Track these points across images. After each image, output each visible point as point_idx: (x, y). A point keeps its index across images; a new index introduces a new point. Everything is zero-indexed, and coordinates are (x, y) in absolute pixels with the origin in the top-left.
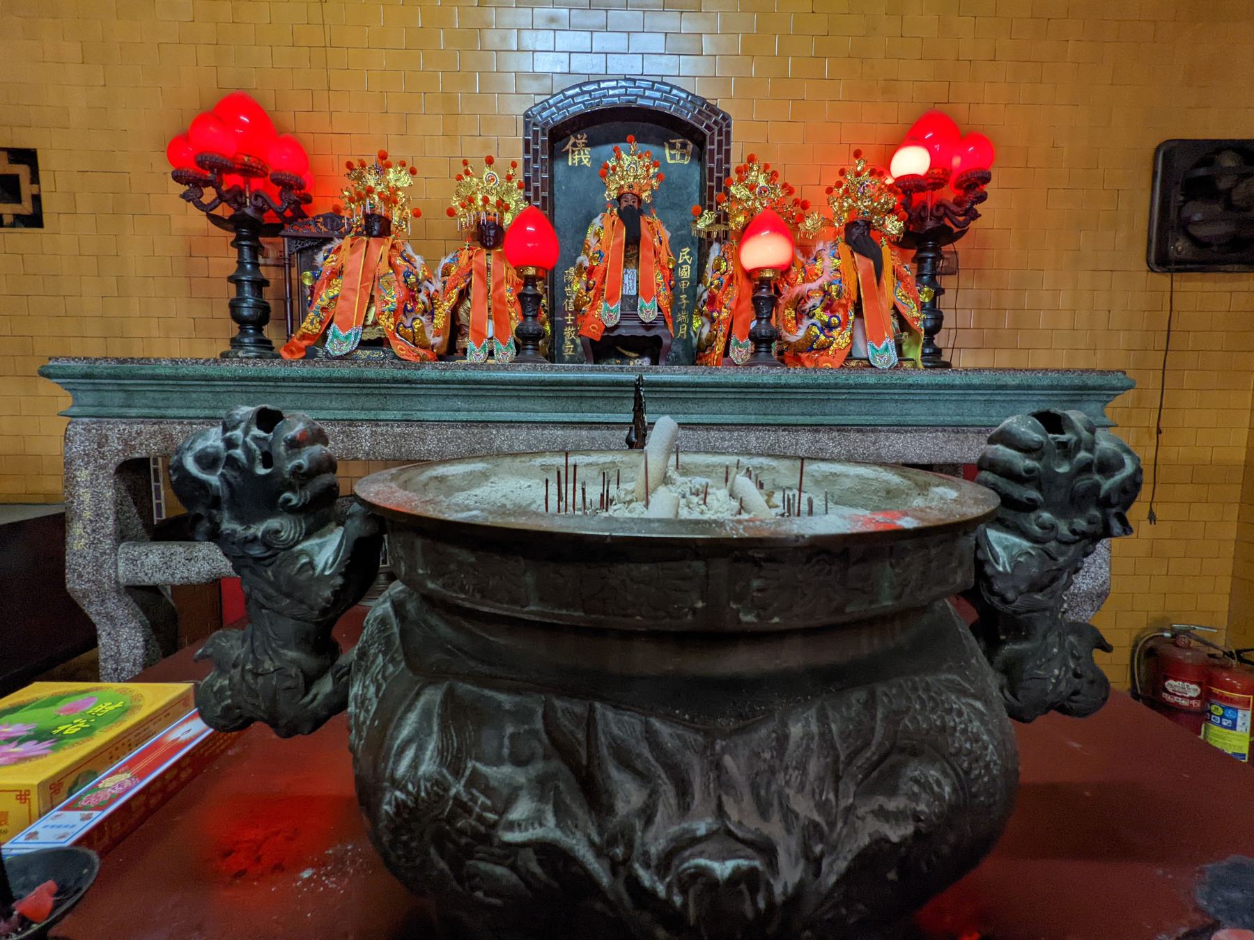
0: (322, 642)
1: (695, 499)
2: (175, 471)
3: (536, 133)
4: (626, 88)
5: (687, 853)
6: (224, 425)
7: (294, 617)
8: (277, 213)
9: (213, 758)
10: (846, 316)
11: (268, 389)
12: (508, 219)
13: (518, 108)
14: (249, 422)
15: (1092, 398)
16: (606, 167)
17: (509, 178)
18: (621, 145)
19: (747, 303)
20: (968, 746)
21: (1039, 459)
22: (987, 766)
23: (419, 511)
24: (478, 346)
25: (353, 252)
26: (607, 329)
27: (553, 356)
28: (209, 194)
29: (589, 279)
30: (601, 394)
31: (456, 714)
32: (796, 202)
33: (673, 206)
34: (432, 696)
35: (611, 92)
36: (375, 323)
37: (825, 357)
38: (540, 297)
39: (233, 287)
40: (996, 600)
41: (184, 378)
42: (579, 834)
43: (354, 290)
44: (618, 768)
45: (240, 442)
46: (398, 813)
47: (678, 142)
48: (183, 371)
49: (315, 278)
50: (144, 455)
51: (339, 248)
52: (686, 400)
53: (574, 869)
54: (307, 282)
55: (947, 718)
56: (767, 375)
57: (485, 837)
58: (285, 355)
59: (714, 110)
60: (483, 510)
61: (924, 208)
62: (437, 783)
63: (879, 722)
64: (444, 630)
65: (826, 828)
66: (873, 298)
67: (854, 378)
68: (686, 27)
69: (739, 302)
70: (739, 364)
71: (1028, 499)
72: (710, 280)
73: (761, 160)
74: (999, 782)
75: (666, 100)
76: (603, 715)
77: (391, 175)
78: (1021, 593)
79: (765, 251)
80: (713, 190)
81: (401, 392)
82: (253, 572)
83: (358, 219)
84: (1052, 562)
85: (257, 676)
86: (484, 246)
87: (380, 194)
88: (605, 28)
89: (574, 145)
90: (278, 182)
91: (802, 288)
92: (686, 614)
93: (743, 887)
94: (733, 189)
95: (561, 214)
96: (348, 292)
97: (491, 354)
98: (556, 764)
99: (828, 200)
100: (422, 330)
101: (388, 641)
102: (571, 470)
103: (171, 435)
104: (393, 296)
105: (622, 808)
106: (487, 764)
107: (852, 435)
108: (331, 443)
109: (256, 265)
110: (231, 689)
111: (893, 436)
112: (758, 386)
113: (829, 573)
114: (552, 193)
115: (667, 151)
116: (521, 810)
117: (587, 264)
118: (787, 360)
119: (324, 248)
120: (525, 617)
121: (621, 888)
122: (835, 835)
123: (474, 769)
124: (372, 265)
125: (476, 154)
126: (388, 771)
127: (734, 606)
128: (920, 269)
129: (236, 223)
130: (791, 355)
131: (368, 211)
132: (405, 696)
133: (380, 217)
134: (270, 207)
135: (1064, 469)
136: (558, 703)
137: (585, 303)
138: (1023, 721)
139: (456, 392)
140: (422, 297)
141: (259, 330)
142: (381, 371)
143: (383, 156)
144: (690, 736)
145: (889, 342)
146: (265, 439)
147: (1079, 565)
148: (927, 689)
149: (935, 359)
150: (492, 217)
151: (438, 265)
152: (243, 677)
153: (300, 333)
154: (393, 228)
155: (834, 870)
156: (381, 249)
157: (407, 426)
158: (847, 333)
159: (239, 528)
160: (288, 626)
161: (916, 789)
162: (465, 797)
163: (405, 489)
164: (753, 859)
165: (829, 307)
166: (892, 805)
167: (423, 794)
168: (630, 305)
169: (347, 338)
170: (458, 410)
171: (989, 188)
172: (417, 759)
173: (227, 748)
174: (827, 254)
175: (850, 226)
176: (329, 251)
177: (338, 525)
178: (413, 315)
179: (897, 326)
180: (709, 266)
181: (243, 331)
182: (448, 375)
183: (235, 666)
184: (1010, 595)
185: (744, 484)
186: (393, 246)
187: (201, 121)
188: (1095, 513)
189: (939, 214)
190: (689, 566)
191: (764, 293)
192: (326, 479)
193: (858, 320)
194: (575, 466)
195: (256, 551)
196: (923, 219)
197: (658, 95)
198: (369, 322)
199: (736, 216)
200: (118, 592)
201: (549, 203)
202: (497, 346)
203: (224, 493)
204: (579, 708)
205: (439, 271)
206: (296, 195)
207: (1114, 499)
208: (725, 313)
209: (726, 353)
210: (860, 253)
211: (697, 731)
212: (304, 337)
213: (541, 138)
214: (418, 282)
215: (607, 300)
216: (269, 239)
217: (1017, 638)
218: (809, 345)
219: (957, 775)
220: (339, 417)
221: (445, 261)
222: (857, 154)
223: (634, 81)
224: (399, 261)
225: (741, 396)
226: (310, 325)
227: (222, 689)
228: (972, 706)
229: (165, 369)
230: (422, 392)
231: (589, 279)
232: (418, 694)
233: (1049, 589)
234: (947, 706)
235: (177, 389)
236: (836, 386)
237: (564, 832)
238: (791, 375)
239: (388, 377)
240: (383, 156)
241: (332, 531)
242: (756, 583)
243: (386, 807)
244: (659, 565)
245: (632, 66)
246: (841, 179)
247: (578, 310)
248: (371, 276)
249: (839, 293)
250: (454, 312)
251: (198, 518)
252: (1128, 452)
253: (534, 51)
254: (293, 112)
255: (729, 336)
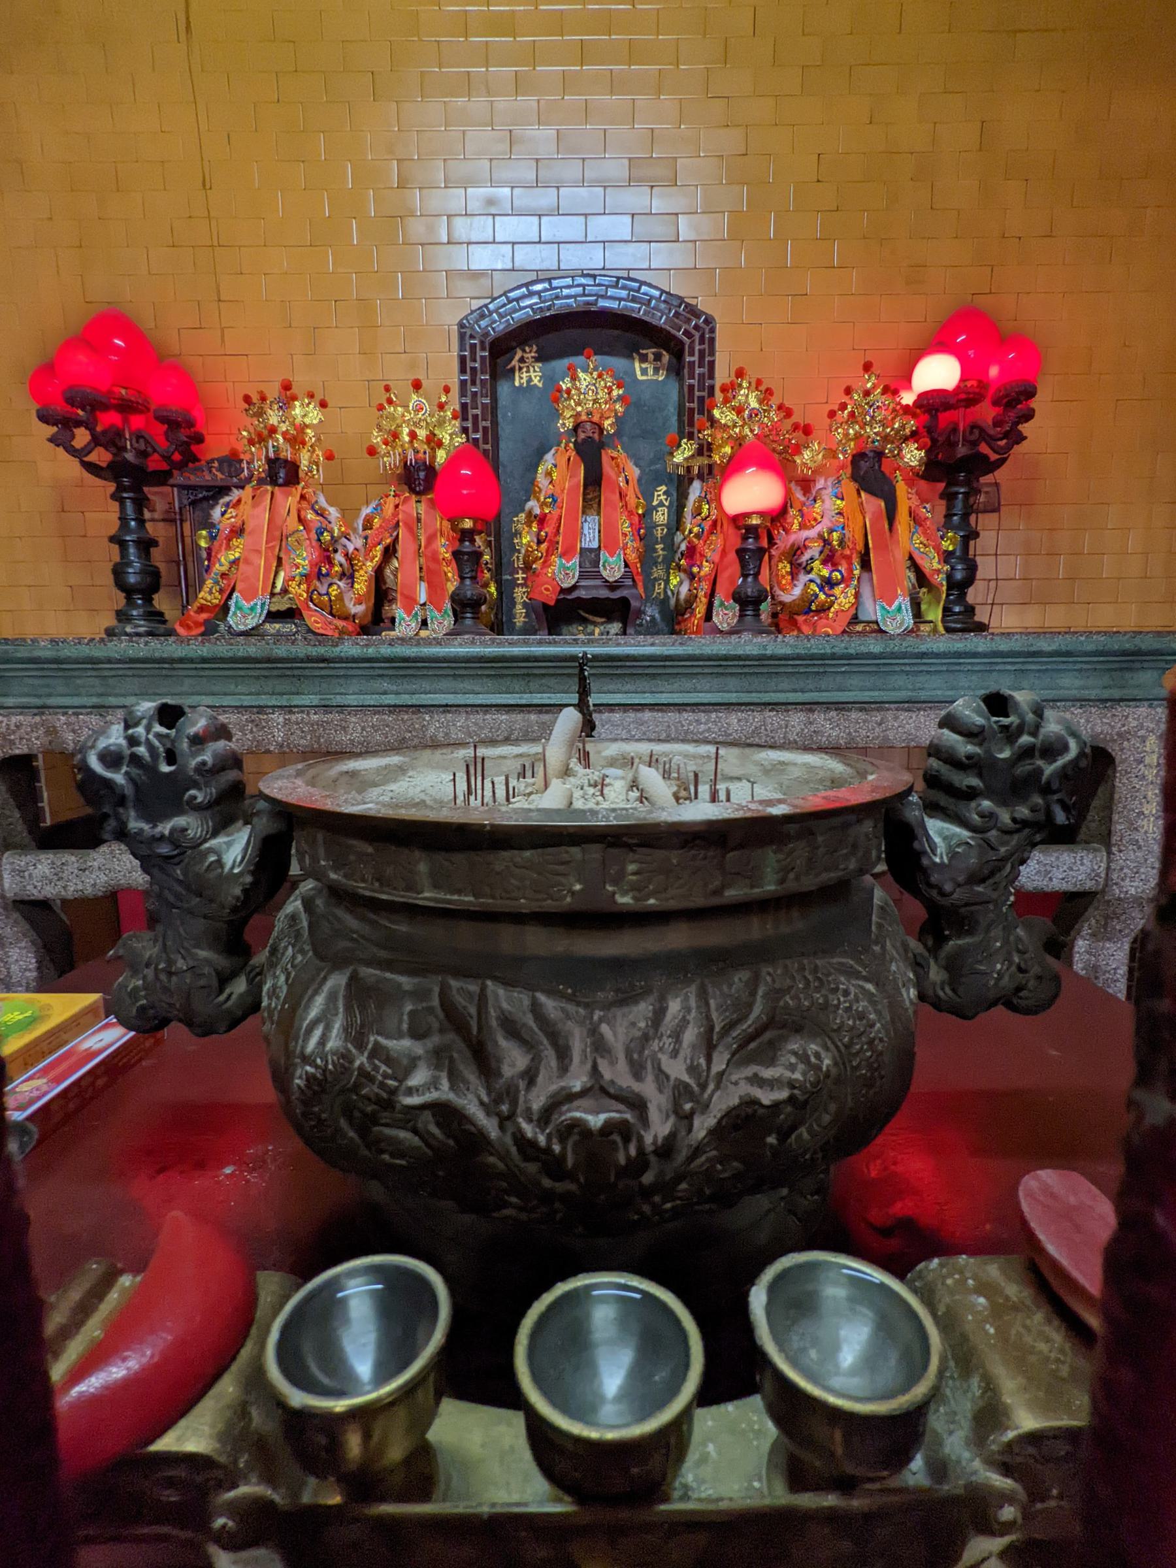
0: (236, 939)
1: (591, 790)
2: (79, 770)
3: (473, 346)
4: (584, 286)
5: (565, 1108)
6: (126, 721)
7: (205, 917)
8: (163, 457)
9: (128, 1067)
10: (850, 570)
11: (164, 672)
12: (441, 456)
13: (451, 317)
14: (151, 719)
15: (1146, 665)
16: (559, 390)
17: (441, 406)
18: (579, 360)
19: (732, 556)
20: (850, 1022)
21: (980, 745)
22: (871, 1042)
23: (319, 805)
24: (409, 613)
25: (254, 506)
26: (563, 591)
27: (499, 627)
28: (82, 437)
29: (540, 530)
30: (551, 671)
31: (360, 995)
32: (796, 427)
33: (646, 434)
34: (337, 981)
35: (566, 292)
36: (285, 591)
37: (824, 621)
38: (479, 555)
39: (115, 548)
40: (934, 893)
41: (67, 661)
42: (470, 1096)
43: (259, 552)
44: (506, 1038)
45: (143, 739)
46: (308, 1086)
47: (650, 352)
48: (66, 652)
49: (212, 538)
50: (25, 751)
51: (239, 501)
52: (654, 676)
53: (468, 1127)
54: (203, 544)
55: (831, 997)
56: (750, 644)
57: (388, 1103)
58: (181, 630)
59: (694, 311)
60: (377, 803)
61: (955, 430)
62: (343, 1056)
63: (759, 998)
64: (351, 922)
65: (696, 1089)
66: (884, 548)
67: (855, 646)
68: (659, 205)
69: (724, 553)
70: (723, 634)
71: (968, 787)
72: (689, 526)
73: (752, 374)
74: (886, 1058)
75: (634, 300)
76: (497, 996)
77: (297, 411)
78: (959, 885)
79: (750, 493)
80: (694, 414)
81: (317, 673)
82: (162, 869)
83: (260, 466)
84: (991, 853)
85: (170, 974)
86: (412, 490)
87: (284, 434)
88: (557, 212)
89: (522, 360)
90: (163, 420)
91: (798, 535)
92: (565, 896)
93: (616, 1137)
94: (716, 413)
95: (508, 450)
96: (253, 556)
97: (424, 623)
98: (451, 1036)
99: (831, 426)
100: (340, 597)
101: (298, 935)
102: (479, 761)
103: (54, 727)
104: (303, 558)
105: (508, 1071)
106: (388, 1037)
107: (854, 715)
108: (237, 735)
109: (141, 522)
110: (145, 989)
111: (903, 715)
112: (738, 658)
113: (705, 858)
114: (495, 423)
115: (637, 365)
116: (418, 1078)
117: (537, 511)
118: (782, 625)
119: (221, 501)
120: (420, 903)
121: (508, 1140)
122: (706, 1096)
123: (376, 1043)
124: (279, 522)
125: (400, 379)
126: (299, 1048)
127: (610, 888)
128: (949, 507)
129: (115, 471)
130: (786, 619)
131: (271, 455)
132: (313, 980)
133: (286, 461)
134: (155, 450)
135: (1005, 754)
136: (454, 983)
137: (536, 559)
138: (964, 1017)
139: (381, 672)
140: (339, 558)
141: (148, 600)
142: (293, 649)
143: (287, 386)
144: (571, 1008)
145: (903, 601)
146: (167, 736)
147: (1026, 855)
148: (815, 970)
149: (962, 620)
150: (421, 455)
151: (359, 516)
152: (157, 978)
153: (196, 605)
154: (301, 474)
155: (702, 1126)
156: (289, 501)
157: (326, 713)
158: (851, 591)
159: (146, 827)
160: (199, 925)
161: (793, 1060)
162: (368, 1068)
163: (313, 786)
164: (624, 1112)
165: (829, 559)
166: (768, 1073)
167: (330, 1067)
168: (591, 558)
169: (252, 609)
170: (385, 693)
171: (1035, 403)
172: (324, 1034)
173: (140, 1060)
174: (828, 494)
175: (858, 457)
176: (227, 505)
177: (246, 823)
178: (330, 580)
179: (914, 580)
180: (688, 510)
181: (129, 598)
182: (371, 651)
183: (148, 965)
184: (948, 887)
185: (651, 777)
186: (303, 497)
187: (69, 346)
188: (1038, 800)
189: (973, 438)
190: (567, 852)
191: (751, 543)
192: (232, 775)
193: (866, 575)
194: (483, 759)
195: (164, 849)
196: (953, 445)
197: (624, 293)
198: (278, 589)
199: (721, 446)
200: (5, 909)
201: (493, 434)
202: (432, 613)
203: (129, 791)
204: (473, 987)
205: (360, 523)
206: (185, 437)
207: (1055, 786)
208: (707, 568)
209: (708, 617)
210: (865, 491)
211: (578, 1004)
212: (202, 609)
213: (479, 353)
214: (334, 540)
215: (563, 555)
216: (156, 489)
217: (961, 933)
218: (806, 606)
219: (837, 1047)
220: (245, 703)
221: (366, 511)
222: (867, 367)
223: (594, 277)
224: (310, 516)
225: (720, 670)
226: (208, 594)
227: (136, 988)
228: (862, 987)
229: (44, 651)
230: (342, 672)
231: (540, 530)
232: (325, 979)
233: (991, 881)
234: (832, 986)
235: (60, 674)
236: (833, 656)
237: (457, 1095)
238: (784, 644)
239: (301, 655)
240: (287, 386)
241: (239, 830)
242: (632, 867)
243: (297, 1081)
244: (539, 850)
245: (593, 258)
246: (845, 399)
247: (527, 567)
248: (278, 534)
249: (841, 542)
250: (379, 573)
251: (106, 816)
252: (1074, 734)
253: (469, 243)
254: (171, 317)
255: (711, 595)
